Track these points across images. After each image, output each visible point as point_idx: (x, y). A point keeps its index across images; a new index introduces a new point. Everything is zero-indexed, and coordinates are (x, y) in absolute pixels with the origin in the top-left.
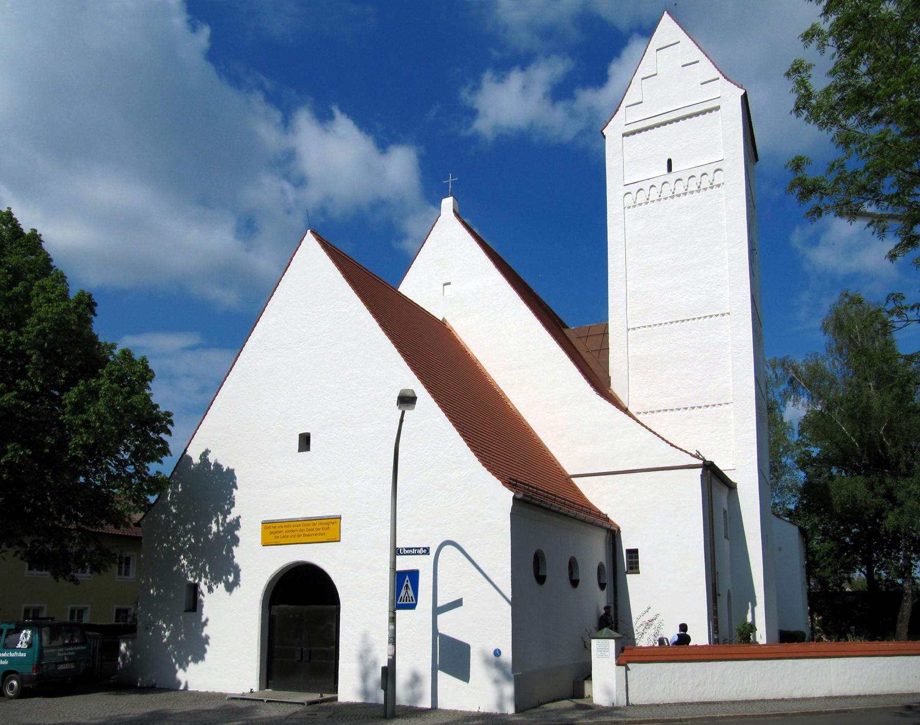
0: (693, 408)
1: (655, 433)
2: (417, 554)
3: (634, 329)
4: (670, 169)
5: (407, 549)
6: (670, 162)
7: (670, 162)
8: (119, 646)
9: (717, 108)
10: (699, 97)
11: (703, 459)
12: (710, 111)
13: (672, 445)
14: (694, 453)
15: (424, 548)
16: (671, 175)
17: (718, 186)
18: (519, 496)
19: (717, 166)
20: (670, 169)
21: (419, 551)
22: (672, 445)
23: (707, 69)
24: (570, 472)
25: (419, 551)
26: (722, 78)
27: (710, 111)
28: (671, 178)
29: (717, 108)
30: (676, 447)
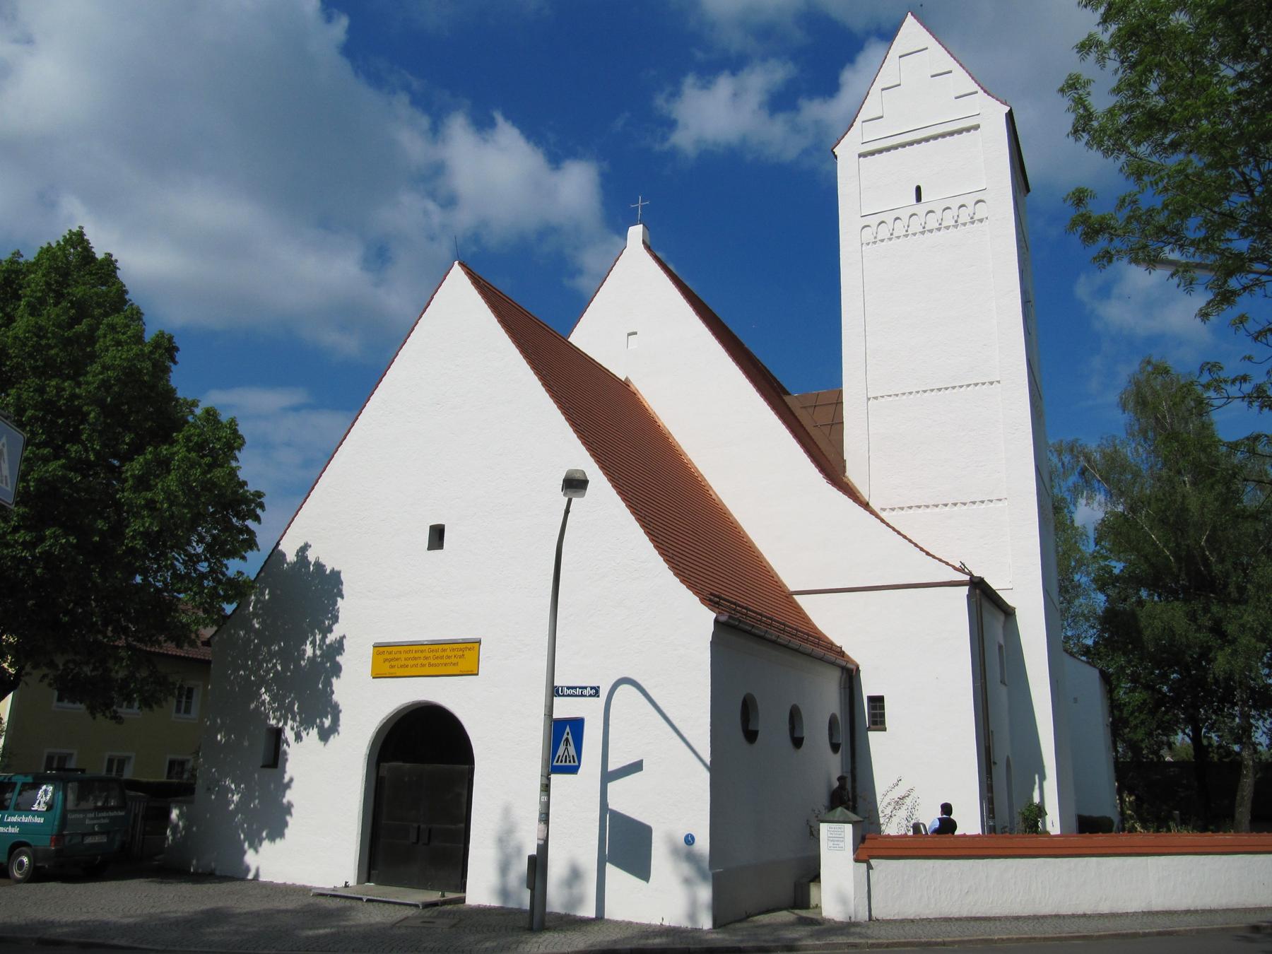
2: (582, 695)
3: (876, 398)
4: (919, 199)
5: (568, 688)
6: (918, 189)
7: (918, 189)
9: (976, 127)
12: (968, 130)
13: (928, 554)
14: (958, 565)
15: (592, 688)
17: (981, 220)
18: (723, 618)
20: (919, 199)
21: (585, 692)
22: (928, 554)
25: (585, 692)
27: (968, 130)
28: (921, 209)
29: (976, 127)
30: (934, 557)
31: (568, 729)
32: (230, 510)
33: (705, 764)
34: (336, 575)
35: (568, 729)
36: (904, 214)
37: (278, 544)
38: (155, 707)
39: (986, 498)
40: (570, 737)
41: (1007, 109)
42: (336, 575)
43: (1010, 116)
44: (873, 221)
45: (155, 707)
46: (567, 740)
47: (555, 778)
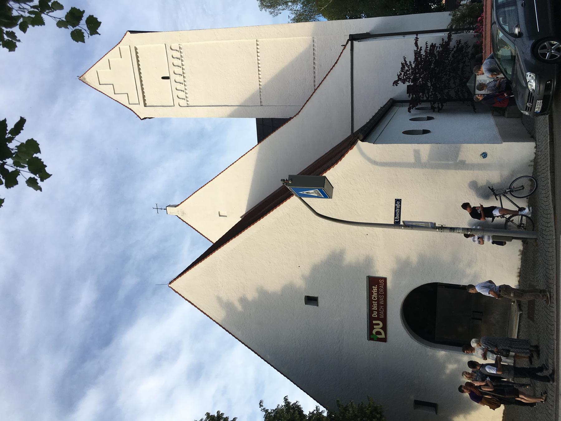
0: (314, 68)
1: (327, 75)
2: (400, 208)
3: (261, 102)
4: (168, 78)
5: (395, 216)
6: (163, 78)
7: (163, 78)
8: (539, 79)
9: (136, 49)
10: (128, 61)
11: (348, 40)
12: (137, 53)
13: (336, 63)
14: (343, 48)
15: (396, 203)
16: (171, 77)
17: (180, 48)
18: (362, 137)
19: (168, 48)
20: (168, 78)
21: (398, 207)
22: (336, 63)
23: (113, 55)
24: (349, 133)
25: (398, 207)
26: (119, 45)
27: (137, 53)
28: (173, 77)
29: (136, 49)
30: (338, 60)
32: (493, 115)
34: (14, 51)
36: (175, 85)
39: (312, 47)
41: (129, 33)
42: (14, 51)
43: (132, 32)
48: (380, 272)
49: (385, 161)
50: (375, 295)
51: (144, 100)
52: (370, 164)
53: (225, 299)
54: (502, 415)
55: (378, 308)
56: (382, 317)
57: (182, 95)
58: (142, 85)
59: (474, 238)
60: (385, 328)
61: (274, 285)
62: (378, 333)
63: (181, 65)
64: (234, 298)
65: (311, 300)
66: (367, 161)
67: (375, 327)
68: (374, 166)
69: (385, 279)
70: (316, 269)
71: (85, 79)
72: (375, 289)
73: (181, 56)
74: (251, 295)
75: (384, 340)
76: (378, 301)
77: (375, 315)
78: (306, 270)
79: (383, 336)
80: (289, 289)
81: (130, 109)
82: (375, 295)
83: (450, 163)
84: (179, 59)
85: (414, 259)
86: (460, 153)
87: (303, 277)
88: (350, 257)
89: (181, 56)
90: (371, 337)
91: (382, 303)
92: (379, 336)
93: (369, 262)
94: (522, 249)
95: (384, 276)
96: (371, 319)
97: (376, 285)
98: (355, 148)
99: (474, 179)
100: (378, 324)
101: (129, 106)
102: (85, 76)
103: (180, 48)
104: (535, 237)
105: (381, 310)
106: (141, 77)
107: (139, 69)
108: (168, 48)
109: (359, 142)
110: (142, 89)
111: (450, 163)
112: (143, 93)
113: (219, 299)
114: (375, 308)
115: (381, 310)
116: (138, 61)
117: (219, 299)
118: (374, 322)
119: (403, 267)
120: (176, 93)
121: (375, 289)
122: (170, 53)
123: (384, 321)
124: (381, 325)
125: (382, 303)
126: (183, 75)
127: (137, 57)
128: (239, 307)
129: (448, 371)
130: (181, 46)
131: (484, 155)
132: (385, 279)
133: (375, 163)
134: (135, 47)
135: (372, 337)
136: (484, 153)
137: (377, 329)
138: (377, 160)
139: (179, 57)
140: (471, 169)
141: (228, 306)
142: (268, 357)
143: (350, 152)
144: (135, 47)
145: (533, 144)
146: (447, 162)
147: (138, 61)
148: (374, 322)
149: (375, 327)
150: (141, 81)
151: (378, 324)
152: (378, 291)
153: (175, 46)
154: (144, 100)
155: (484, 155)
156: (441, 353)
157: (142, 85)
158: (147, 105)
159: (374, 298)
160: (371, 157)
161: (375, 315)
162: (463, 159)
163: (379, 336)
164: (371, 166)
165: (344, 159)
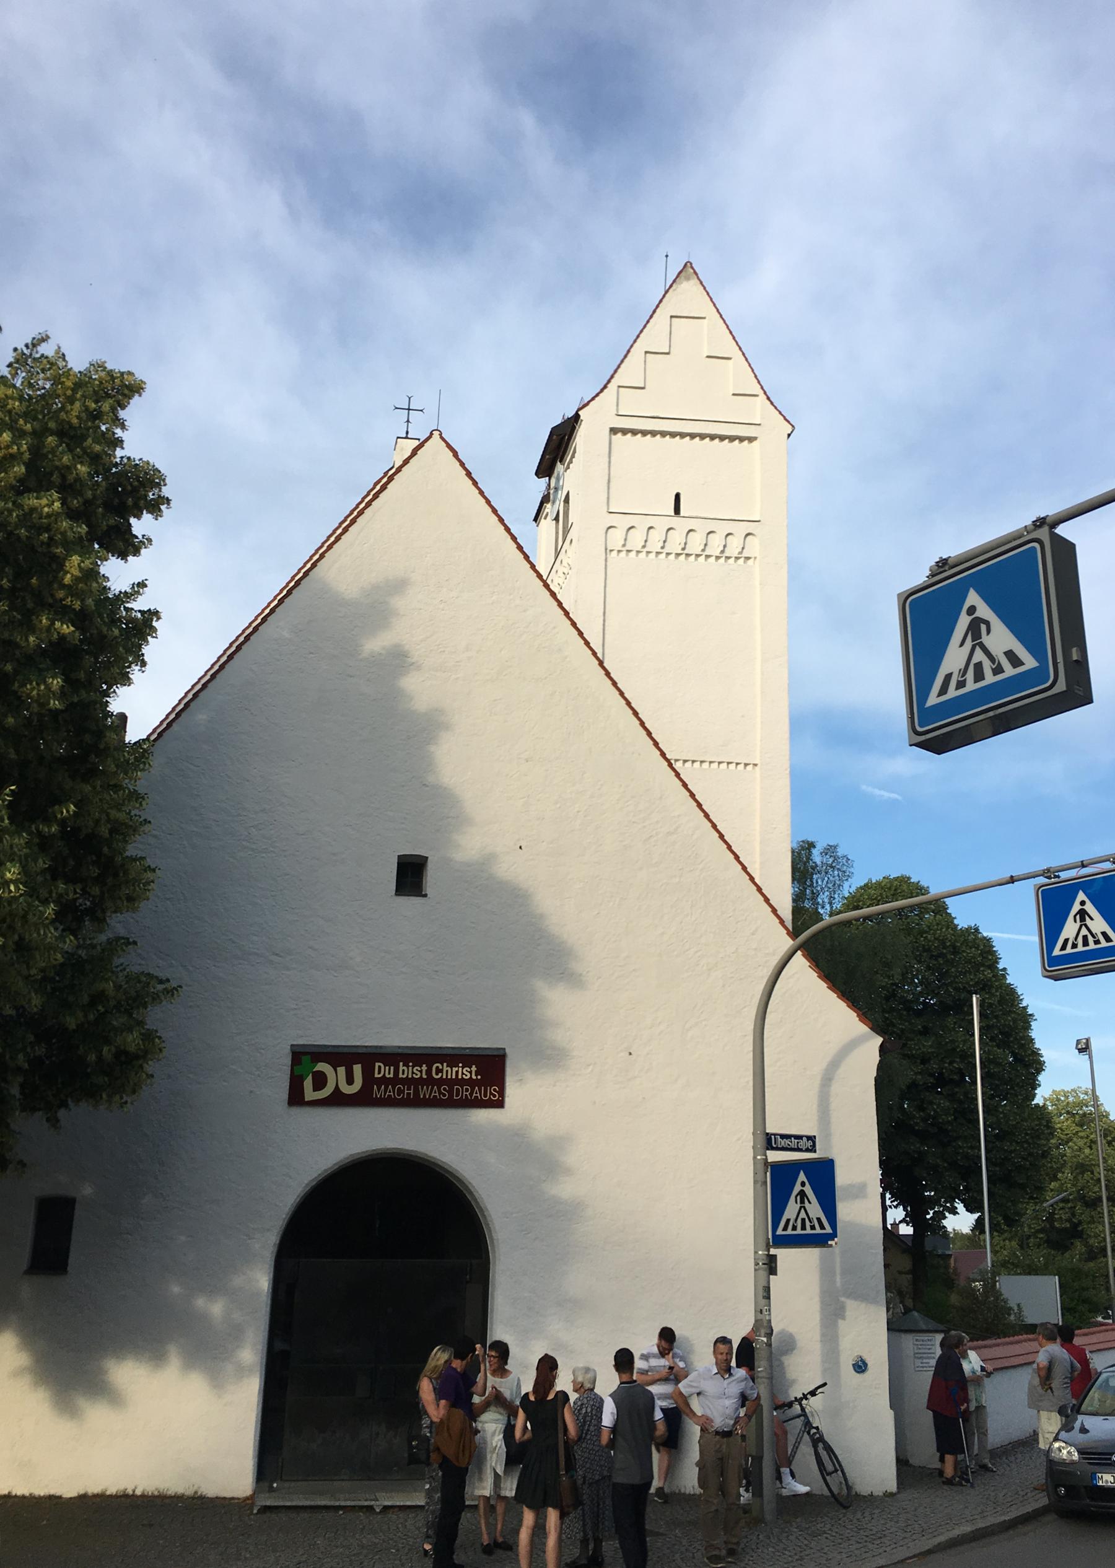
4: (677, 510)
5: (783, 1136)
6: (678, 496)
9: (751, 439)
12: (741, 439)
15: (809, 1138)
17: (748, 558)
19: (750, 528)
20: (677, 510)
27: (741, 439)
28: (675, 521)
29: (751, 439)
31: (802, 1177)
33: (782, 922)
35: (802, 1177)
36: (662, 524)
37: (1091, 1058)
38: (141, 526)
40: (808, 1189)
44: (624, 522)
45: (141, 526)
46: (802, 1194)
47: (784, 1255)
48: (522, 1091)
49: (833, 1106)
50: (449, 1072)
51: (625, 432)
52: (824, 1065)
53: (399, 603)
54: (41, 1492)
55: (408, 1081)
56: (377, 1092)
57: (636, 539)
58: (663, 434)
59: (654, 1356)
60: (338, 1100)
61: (456, 763)
62: (320, 1081)
63: (727, 554)
64: (410, 627)
65: (411, 875)
66: (828, 1059)
67: (342, 1070)
68: (819, 1078)
69: (500, 1104)
70: (514, 898)
71: (688, 279)
72: (467, 1073)
73: (728, 558)
74: (420, 689)
75: (296, 1098)
76: (430, 1081)
77: (382, 1071)
78: (511, 868)
79: (310, 1094)
80: (442, 808)
81: (605, 387)
82: (449, 1072)
83: (838, 1279)
84: (722, 552)
85: (565, 1189)
86: (863, 1305)
87: (490, 858)
88: (558, 1002)
89: (728, 558)
90: (302, 1056)
91: (424, 1092)
92: (308, 1083)
93: (549, 1057)
94: (108, 1493)
95: (507, 1100)
96: (368, 1057)
97: (483, 1077)
98: (863, 1029)
99: (799, 1344)
100: (350, 1081)
101: (612, 386)
102: (694, 281)
103: (748, 558)
104: (768, 1517)
105: (400, 1092)
106: (682, 435)
107: (702, 437)
108: (750, 528)
109: (880, 1040)
110: (654, 433)
111: (838, 1279)
112: (644, 433)
113: (399, 586)
114: (405, 1071)
115: (400, 1092)
116: (722, 438)
117: (399, 586)
118: (357, 1069)
119: (539, 1158)
120: (642, 524)
121: (467, 1073)
122: (741, 529)
123: (363, 1100)
124: (347, 1090)
125: (424, 1092)
126: (684, 553)
127: (732, 439)
128: (375, 644)
129: (200, 1302)
130: (751, 561)
131: (860, 1367)
132: (500, 1104)
133: (828, 1079)
134: (755, 438)
135: (306, 1059)
136: (866, 1365)
137: (336, 1077)
138: (835, 1088)
139: (727, 554)
140: (823, 1335)
141: (376, 607)
142: (200, 716)
143: (851, 1016)
144: (755, 438)
145: (892, 1486)
146: (838, 1270)
147: (722, 438)
148: (357, 1069)
149: (342, 1070)
150: (673, 435)
151: (350, 1081)
152: (462, 1082)
153: (754, 547)
154: (625, 432)
155: (860, 1367)
156: (263, 1281)
157: (663, 434)
158: (613, 437)
159: (438, 1071)
160: (842, 1071)
161: (382, 1071)
162: (847, 1313)
163: (308, 1083)
164: (817, 1069)
165: (832, 996)
